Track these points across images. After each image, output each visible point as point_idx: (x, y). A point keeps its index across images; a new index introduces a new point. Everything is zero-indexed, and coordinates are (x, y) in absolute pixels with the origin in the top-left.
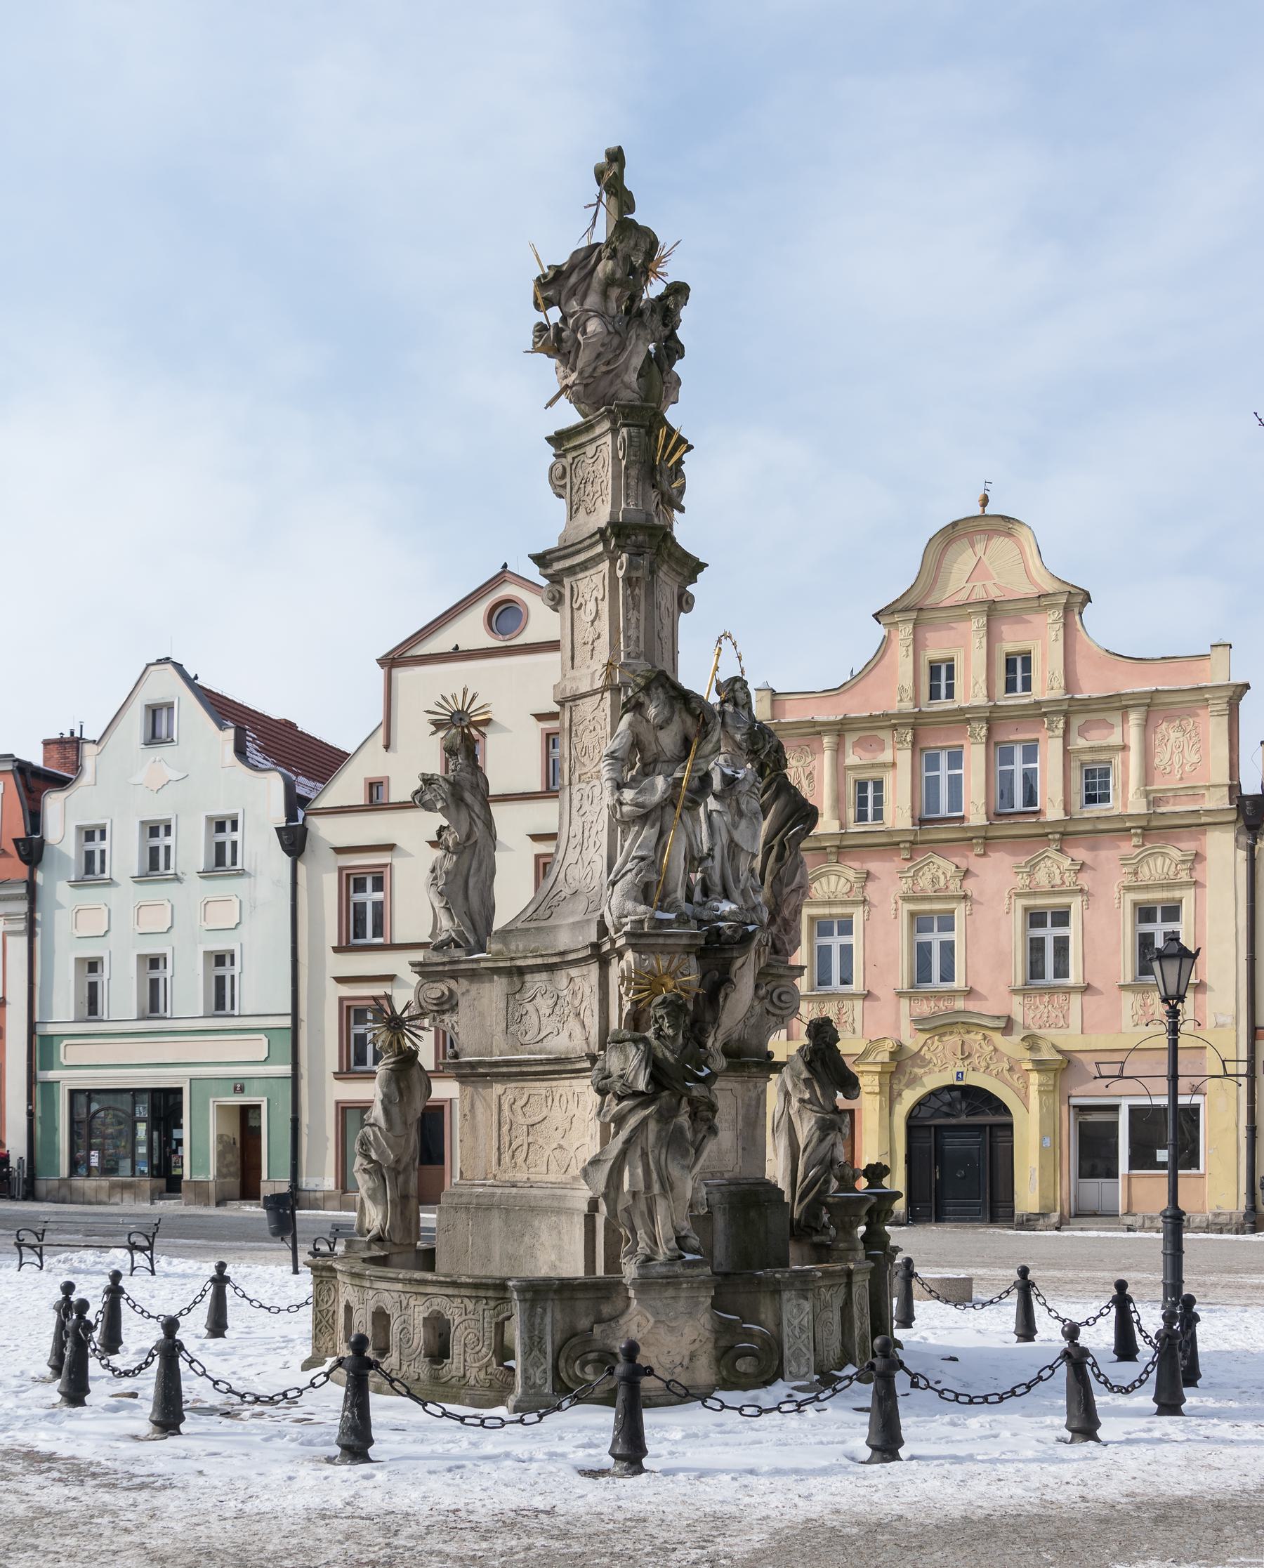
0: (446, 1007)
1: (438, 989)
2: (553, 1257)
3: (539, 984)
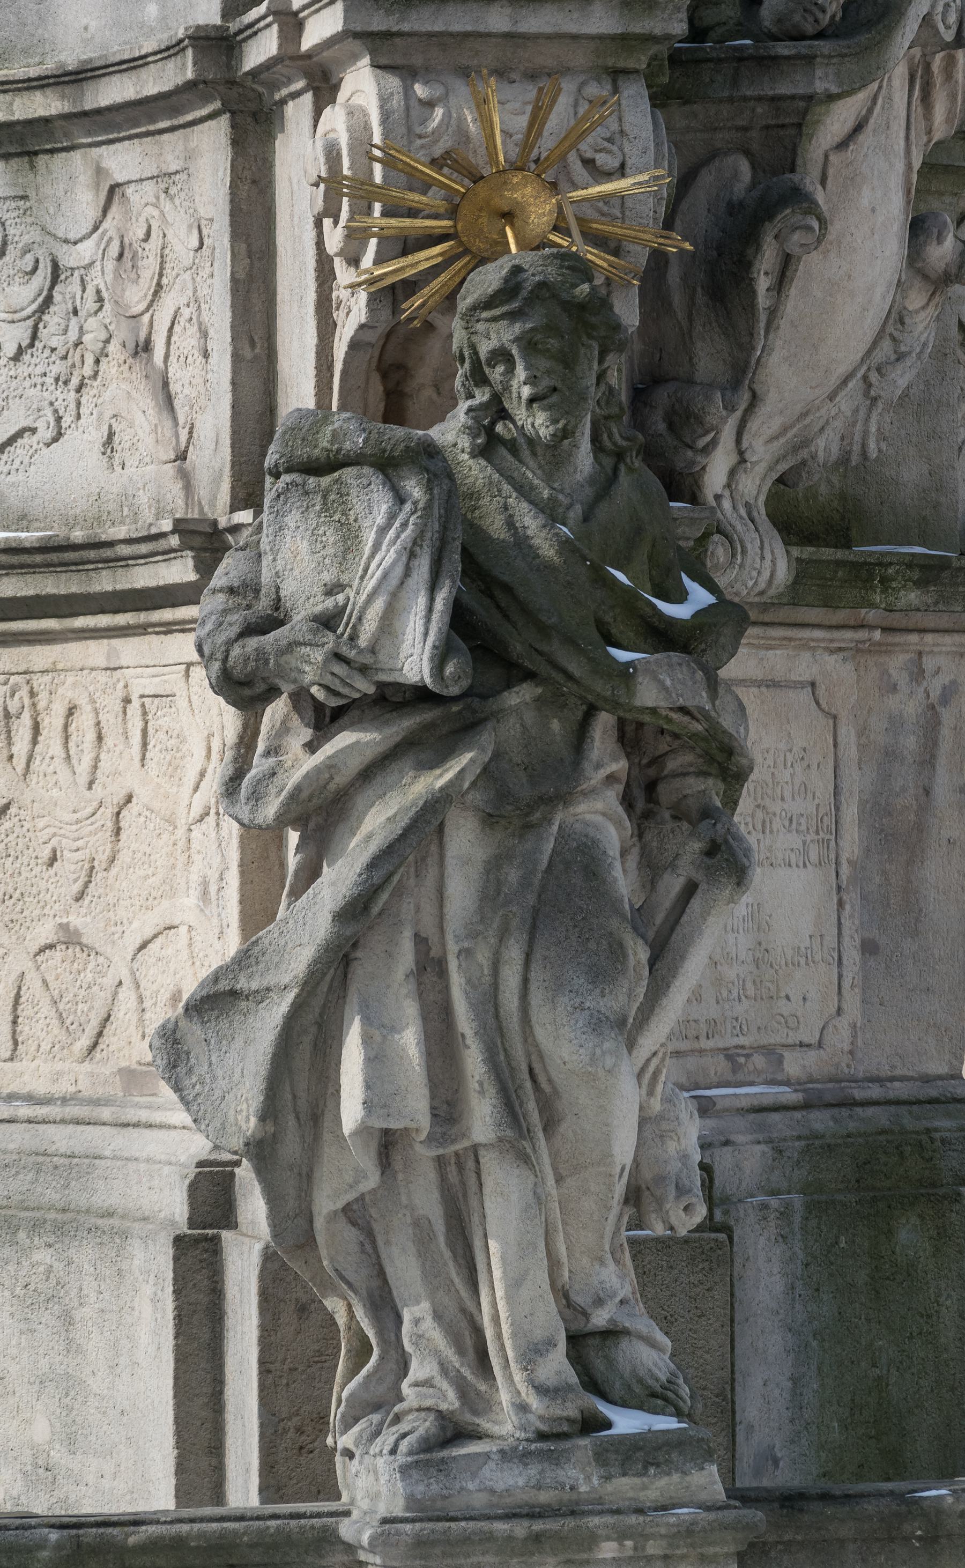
2: (41, 1431)
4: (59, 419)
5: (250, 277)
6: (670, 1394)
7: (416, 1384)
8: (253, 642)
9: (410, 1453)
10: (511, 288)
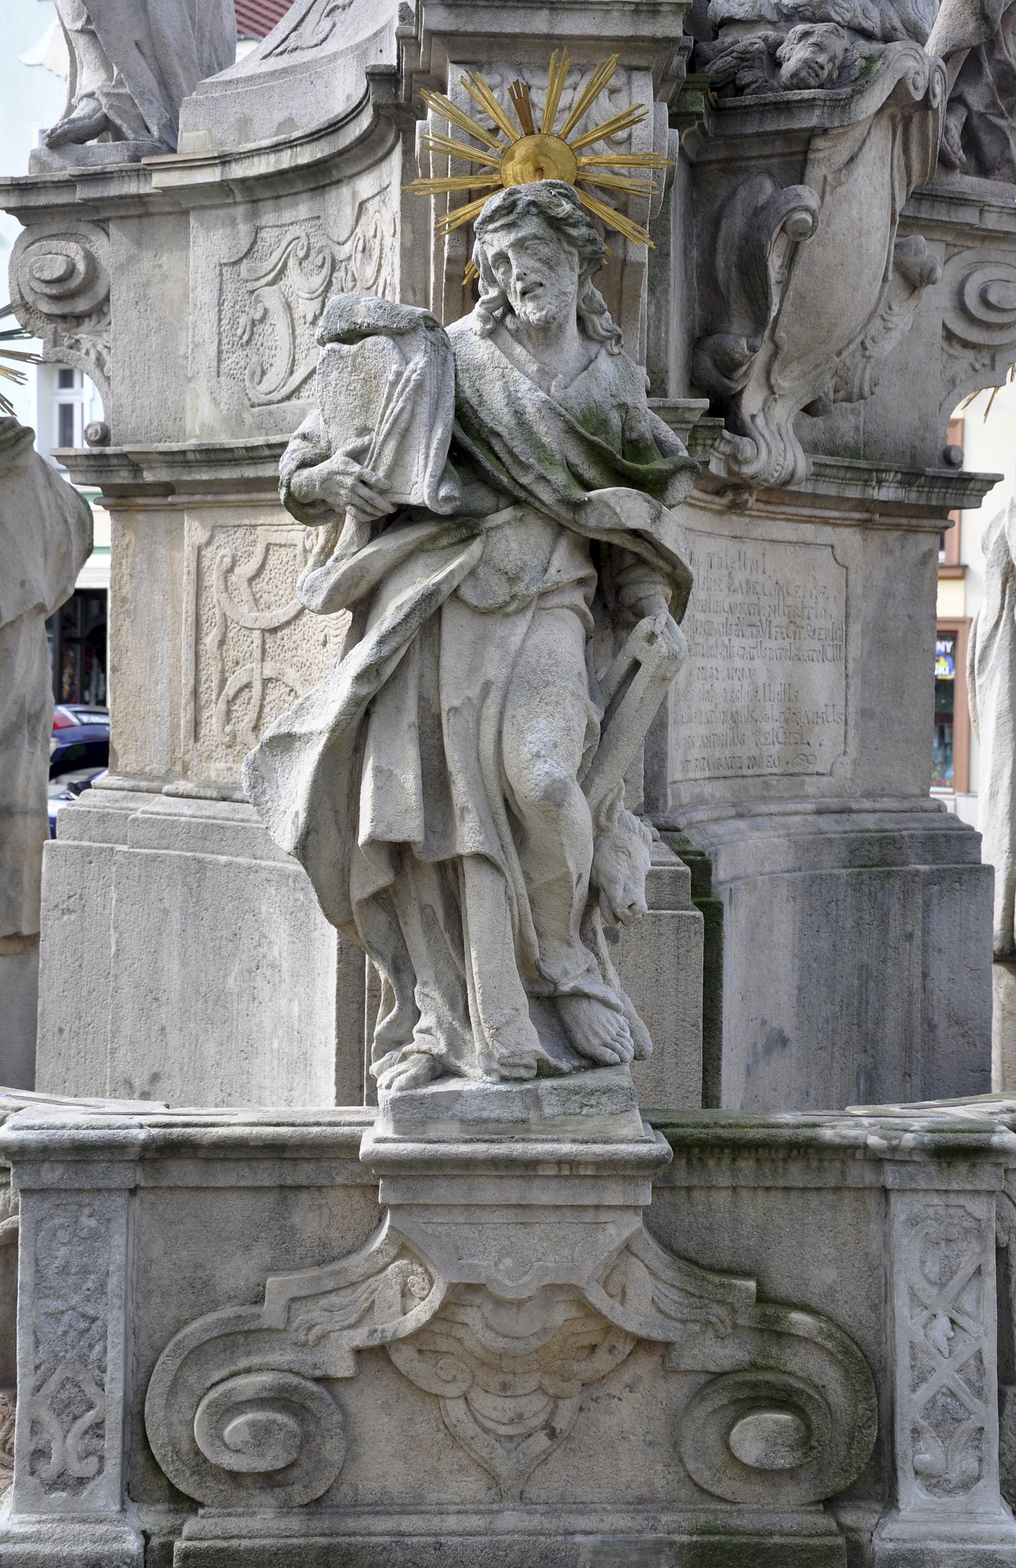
0: (81, 305)
1: (63, 254)
3: (294, 231)
5: (414, 245)
6: (618, 1046)
7: (421, 1031)
8: (306, 472)
9: (401, 1089)
10: (508, 208)
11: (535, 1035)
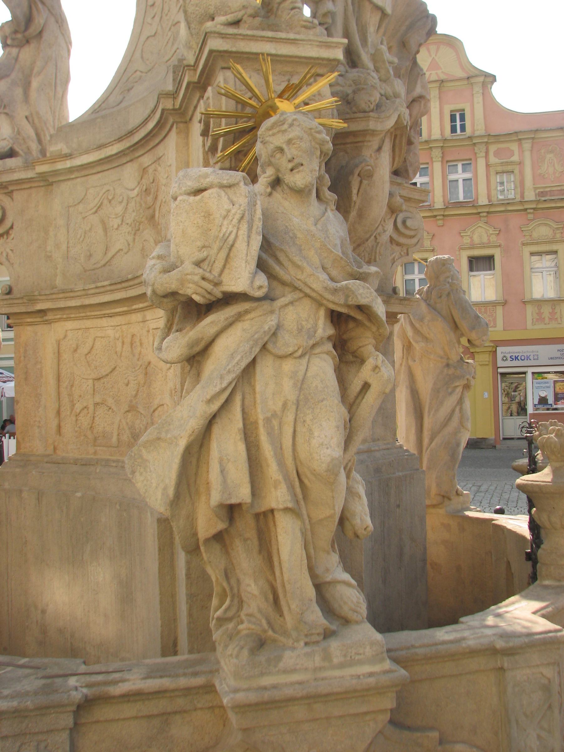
4: (129, 245)
11: (320, 613)
